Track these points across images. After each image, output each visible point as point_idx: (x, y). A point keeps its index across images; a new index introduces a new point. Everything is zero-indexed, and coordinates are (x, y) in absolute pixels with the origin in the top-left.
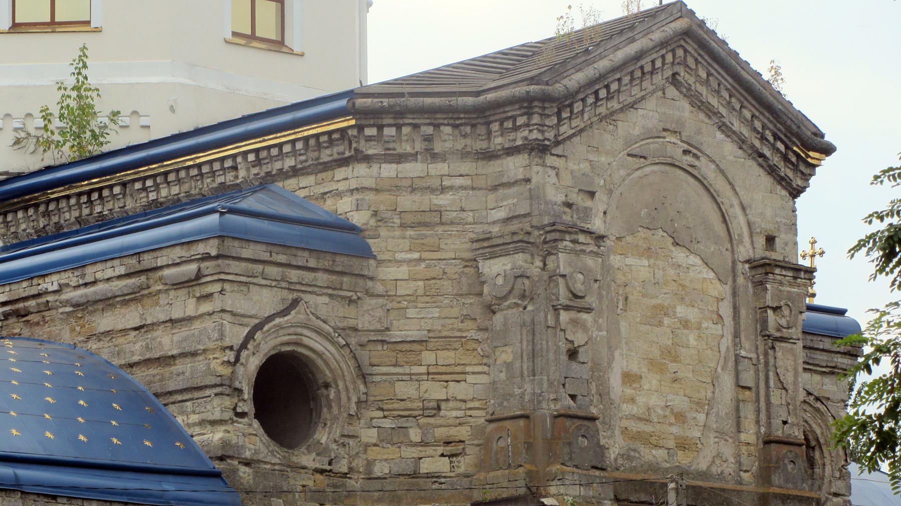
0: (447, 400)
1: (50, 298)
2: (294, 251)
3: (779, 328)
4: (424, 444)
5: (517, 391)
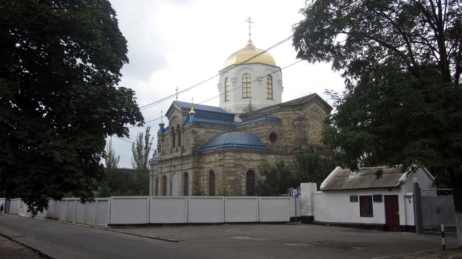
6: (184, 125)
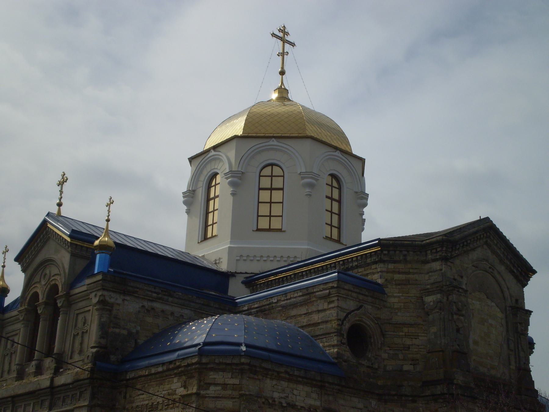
5: (439, 342)
6: (71, 285)
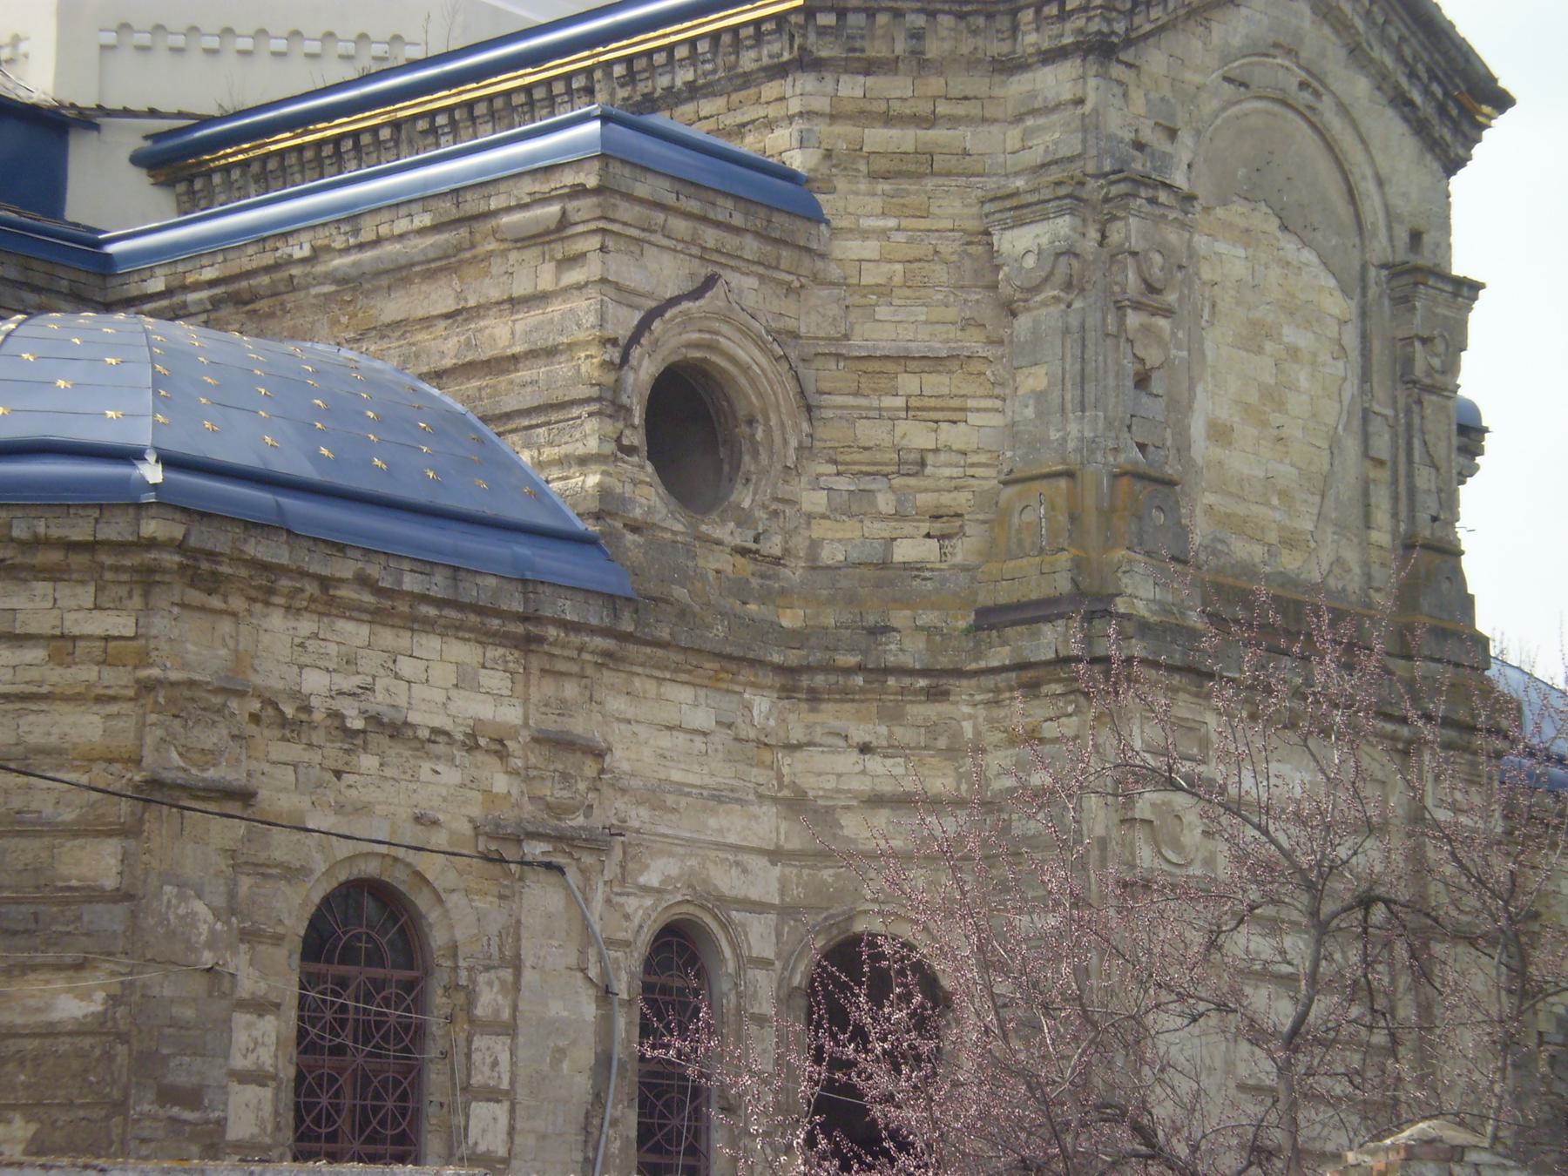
0: (936, 450)
1: (296, 271)
2: (711, 196)
3: (1431, 371)
4: (899, 516)
5: (1054, 435)
